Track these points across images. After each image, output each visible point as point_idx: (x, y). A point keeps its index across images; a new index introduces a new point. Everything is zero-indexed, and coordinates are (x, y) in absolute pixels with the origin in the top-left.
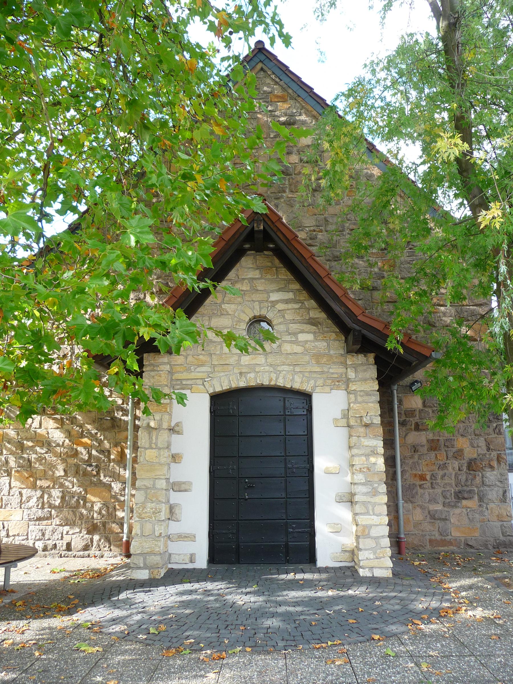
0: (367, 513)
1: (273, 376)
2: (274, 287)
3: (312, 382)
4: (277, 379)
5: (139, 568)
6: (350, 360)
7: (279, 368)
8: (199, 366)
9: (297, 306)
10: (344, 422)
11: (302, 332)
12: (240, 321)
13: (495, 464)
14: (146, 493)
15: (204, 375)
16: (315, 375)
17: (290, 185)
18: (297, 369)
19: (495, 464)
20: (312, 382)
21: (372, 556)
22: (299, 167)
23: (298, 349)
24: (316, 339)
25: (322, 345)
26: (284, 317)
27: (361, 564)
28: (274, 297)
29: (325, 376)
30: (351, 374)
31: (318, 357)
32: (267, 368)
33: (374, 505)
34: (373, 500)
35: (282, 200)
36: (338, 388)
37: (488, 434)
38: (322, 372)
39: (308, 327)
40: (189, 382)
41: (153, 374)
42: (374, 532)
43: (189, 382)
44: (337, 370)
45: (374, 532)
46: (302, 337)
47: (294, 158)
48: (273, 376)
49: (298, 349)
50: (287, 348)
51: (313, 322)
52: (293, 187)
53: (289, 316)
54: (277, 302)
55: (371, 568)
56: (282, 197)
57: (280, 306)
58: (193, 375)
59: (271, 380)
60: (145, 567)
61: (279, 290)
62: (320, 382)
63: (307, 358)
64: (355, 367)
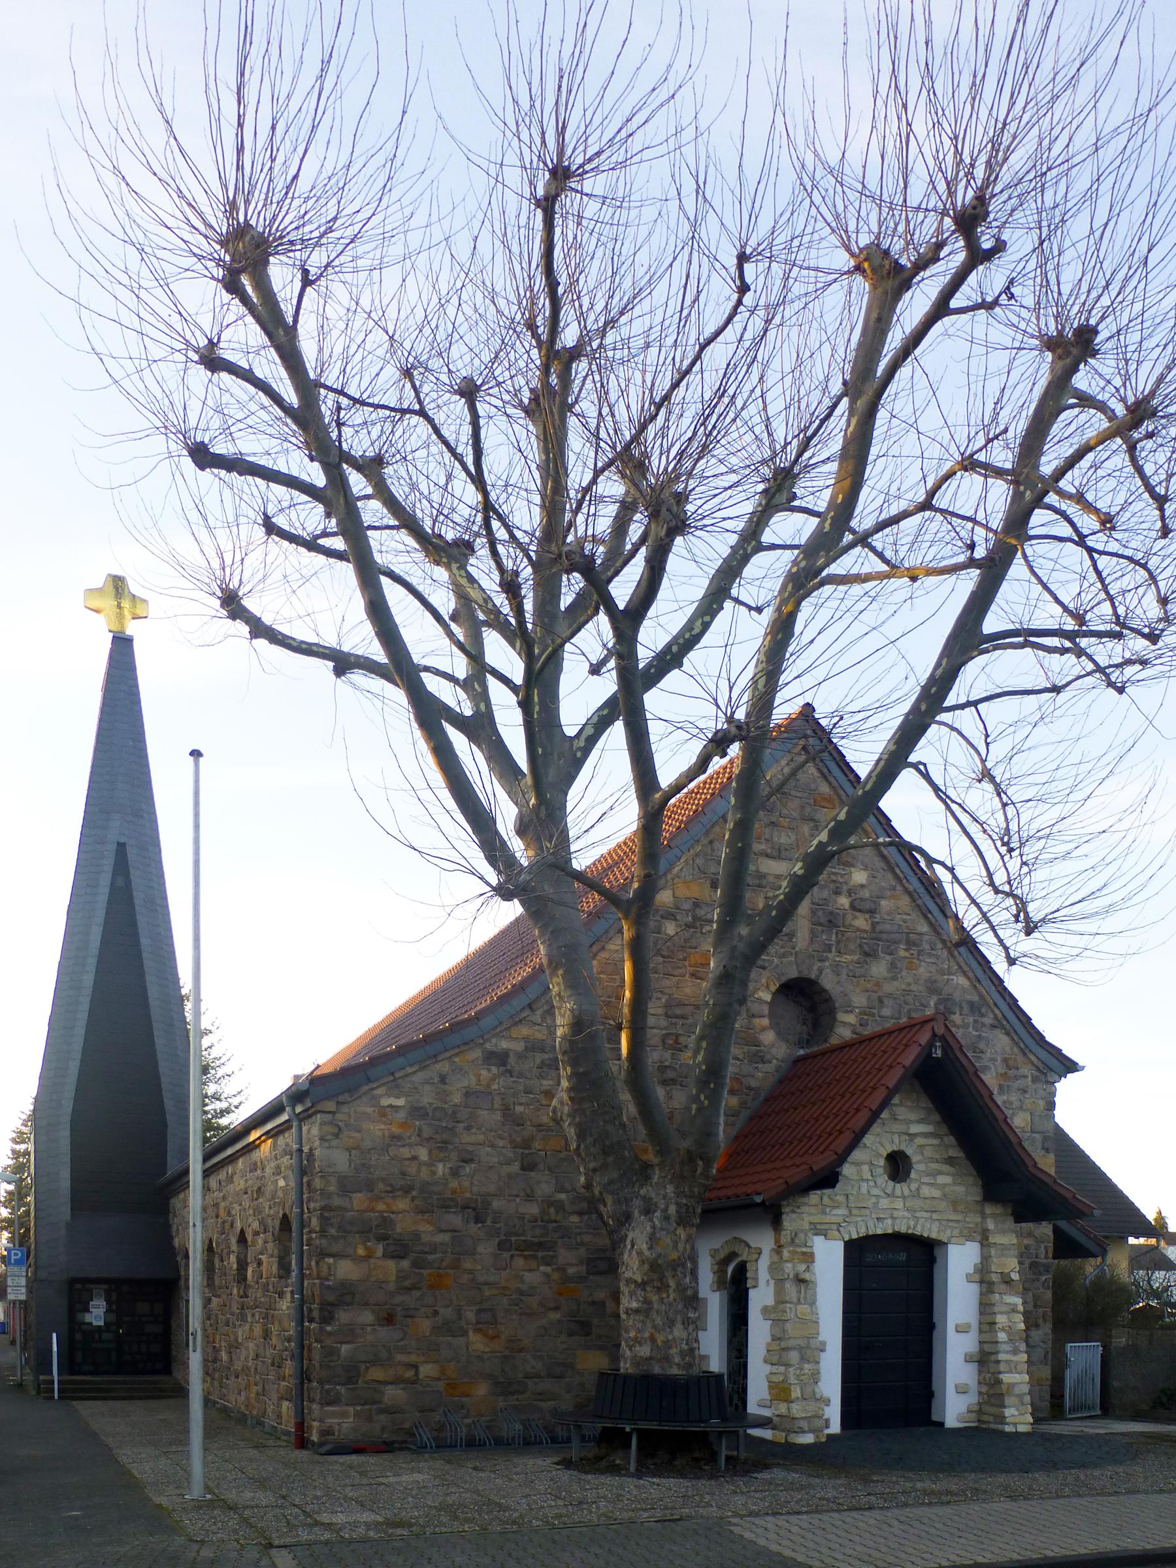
0: (1010, 1372)
1: (912, 1223)
2: (913, 1116)
3: (948, 1233)
4: (915, 1226)
5: (804, 1432)
6: (989, 1209)
7: (918, 1214)
8: (834, 1207)
9: (935, 1142)
10: (977, 1277)
11: (941, 1173)
12: (879, 1155)
13: (1040, 1321)
14: (800, 1353)
15: (840, 1220)
16: (951, 1224)
17: (838, 942)
18: (935, 1216)
19: (1040, 1321)
20: (948, 1233)
21: (1016, 1413)
22: (849, 917)
23: (936, 1193)
24: (955, 1184)
25: (960, 1189)
26: (922, 1153)
27: (1008, 1420)
28: (914, 1129)
29: (961, 1225)
30: (991, 1225)
31: (954, 1204)
32: (905, 1213)
33: (1017, 1363)
34: (1014, 1358)
35: (827, 964)
36: (969, 1239)
37: (1037, 1289)
38: (957, 1221)
39: (946, 1168)
40: (824, 1227)
41: (793, 1216)
42: (1017, 1390)
43: (824, 1227)
44: (974, 1219)
45: (1017, 1390)
46: (941, 1180)
47: (844, 901)
48: (912, 1223)
49: (936, 1193)
50: (926, 1191)
51: (950, 1161)
52: (842, 945)
53: (928, 1152)
54: (916, 1135)
55: (1015, 1424)
56: (827, 959)
57: (919, 1141)
58: (828, 1219)
59: (909, 1228)
60: (811, 1431)
61: (920, 1121)
62: (956, 1232)
63: (944, 1204)
64: (994, 1216)
